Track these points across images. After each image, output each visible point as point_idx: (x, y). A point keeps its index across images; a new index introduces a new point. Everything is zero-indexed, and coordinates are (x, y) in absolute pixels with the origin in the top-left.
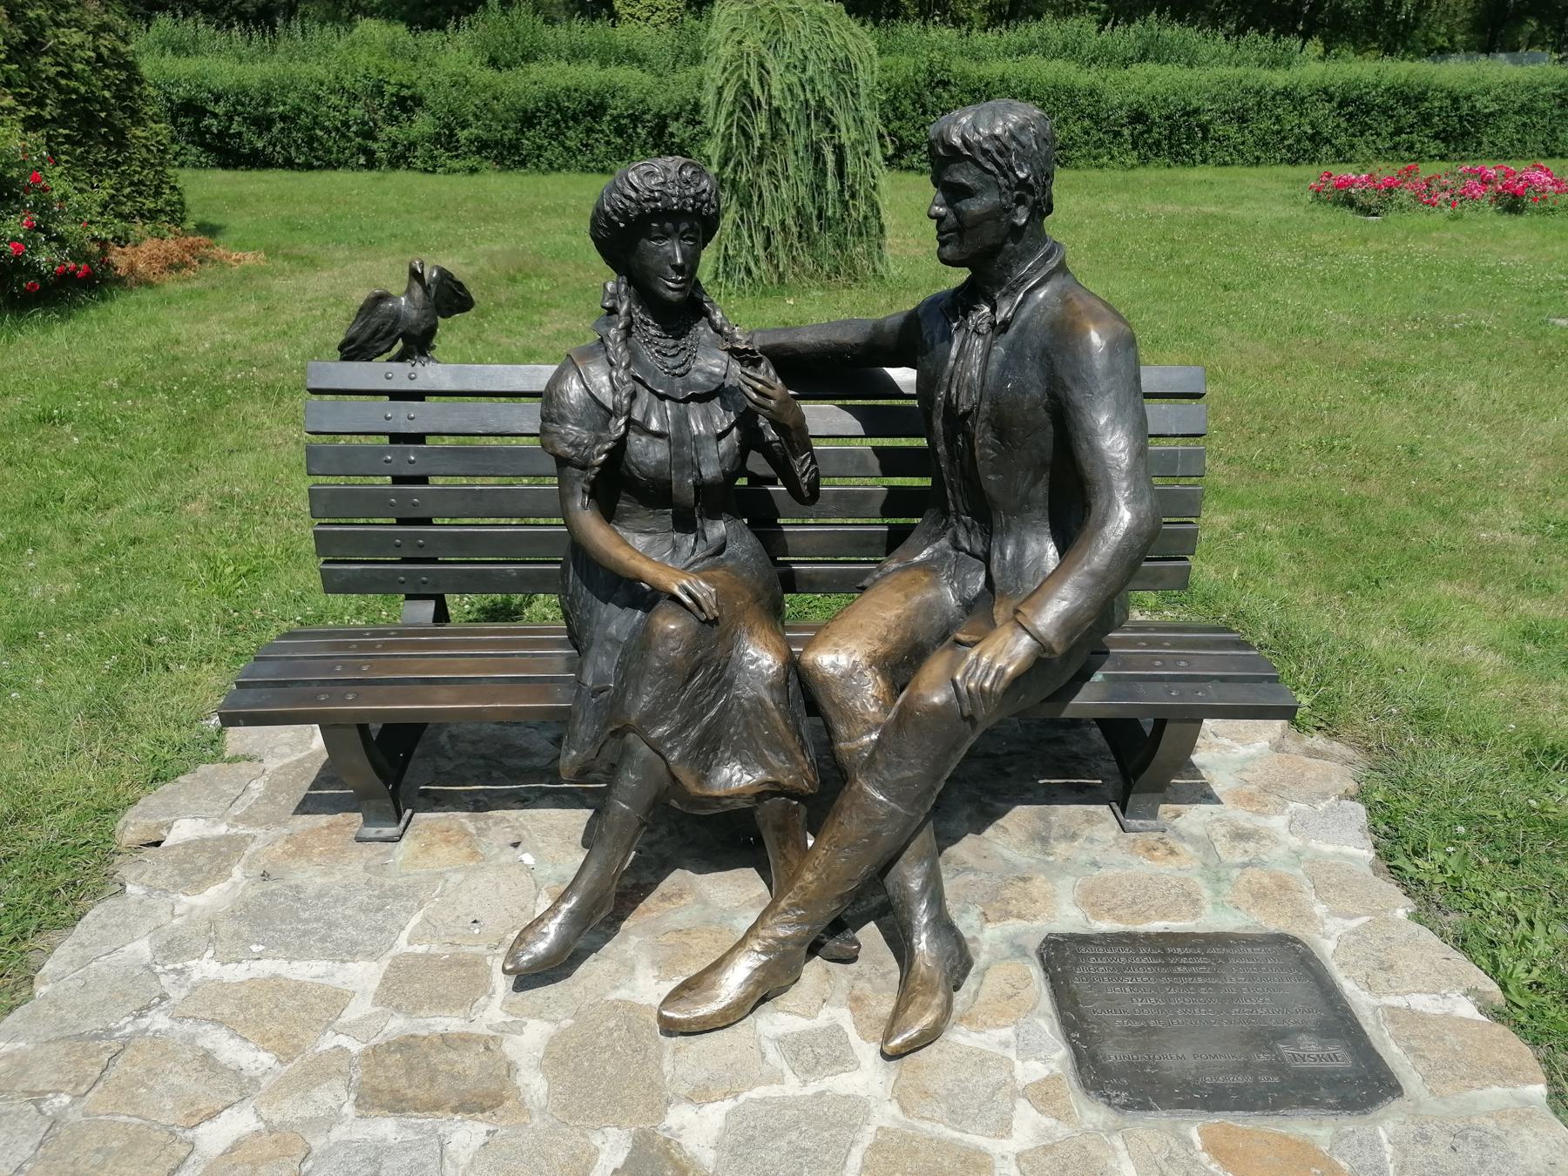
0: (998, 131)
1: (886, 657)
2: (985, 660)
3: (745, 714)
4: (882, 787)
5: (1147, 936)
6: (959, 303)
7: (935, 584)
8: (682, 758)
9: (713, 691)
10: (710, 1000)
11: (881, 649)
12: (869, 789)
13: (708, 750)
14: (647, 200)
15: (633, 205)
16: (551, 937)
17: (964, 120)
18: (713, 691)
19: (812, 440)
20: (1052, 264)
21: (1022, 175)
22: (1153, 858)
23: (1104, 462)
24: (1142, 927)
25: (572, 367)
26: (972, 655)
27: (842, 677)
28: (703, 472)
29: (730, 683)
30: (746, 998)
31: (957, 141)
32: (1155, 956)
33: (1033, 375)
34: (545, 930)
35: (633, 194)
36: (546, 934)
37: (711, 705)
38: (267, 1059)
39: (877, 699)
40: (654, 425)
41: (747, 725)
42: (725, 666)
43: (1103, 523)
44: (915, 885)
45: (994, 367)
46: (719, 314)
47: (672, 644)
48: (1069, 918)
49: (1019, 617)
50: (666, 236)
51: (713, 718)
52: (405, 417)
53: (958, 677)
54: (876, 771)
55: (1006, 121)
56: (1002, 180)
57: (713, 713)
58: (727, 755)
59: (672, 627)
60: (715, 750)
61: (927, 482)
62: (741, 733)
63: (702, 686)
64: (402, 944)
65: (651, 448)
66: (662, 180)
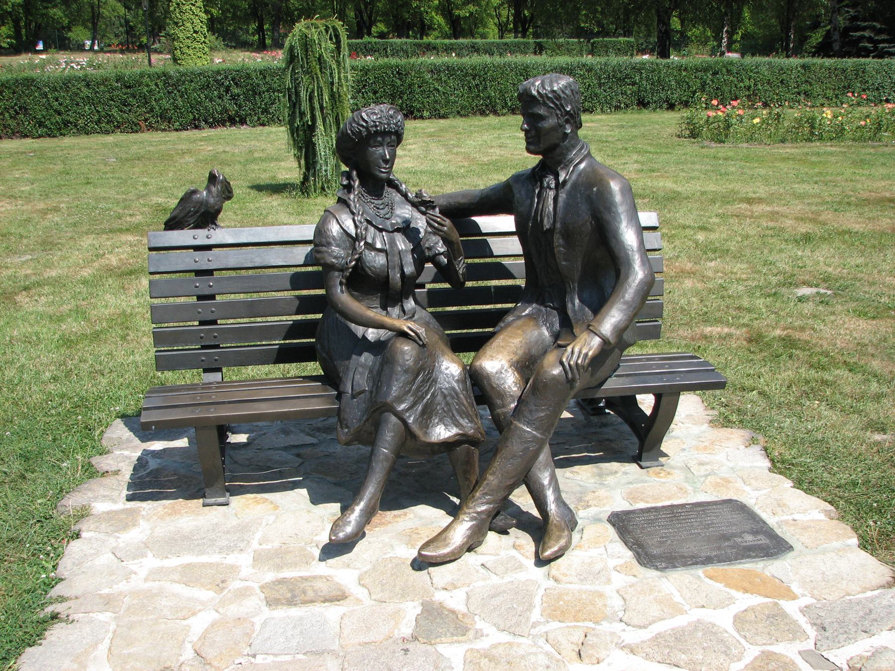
0: (555, 89)
1: (518, 362)
2: (577, 350)
3: (445, 397)
4: (529, 424)
5: (663, 507)
6: (536, 176)
7: (538, 326)
8: (415, 421)
9: (428, 384)
10: (447, 545)
11: (514, 359)
12: (521, 426)
13: (427, 415)
14: (372, 127)
15: (364, 130)
16: (353, 523)
17: (537, 84)
18: (428, 384)
20: (584, 152)
21: (568, 109)
22: (659, 477)
23: (624, 247)
24: (660, 504)
25: (331, 216)
26: (569, 349)
27: (496, 373)
28: (405, 270)
29: (435, 381)
30: (463, 544)
31: (534, 93)
32: (670, 514)
33: (584, 208)
34: (348, 520)
35: (364, 124)
36: (350, 522)
37: (427, 392)
38: (211, 594)
39: (516, 384)
40: (379, 245)
41: (447, 404)
42: (433, 370)
43: (627, 277)
44: (546, 482)
45: (649, 149)
46: (404, 186)
48: (622, 505)
49: (591, 328)
50: (381, 145)
51: (428, 399)
52: (203, 261)
53: (564, 360)
54: (524, 416)
55: (558, 84)
56: (558, 112)
57: (428, 397)
58: (436, 421)
59: (406, 348)
60: (430, 418)
62: (443, 408)
63: (423, 381)
64: (255, 545)
65: (377, 258)
66: (379, 116)
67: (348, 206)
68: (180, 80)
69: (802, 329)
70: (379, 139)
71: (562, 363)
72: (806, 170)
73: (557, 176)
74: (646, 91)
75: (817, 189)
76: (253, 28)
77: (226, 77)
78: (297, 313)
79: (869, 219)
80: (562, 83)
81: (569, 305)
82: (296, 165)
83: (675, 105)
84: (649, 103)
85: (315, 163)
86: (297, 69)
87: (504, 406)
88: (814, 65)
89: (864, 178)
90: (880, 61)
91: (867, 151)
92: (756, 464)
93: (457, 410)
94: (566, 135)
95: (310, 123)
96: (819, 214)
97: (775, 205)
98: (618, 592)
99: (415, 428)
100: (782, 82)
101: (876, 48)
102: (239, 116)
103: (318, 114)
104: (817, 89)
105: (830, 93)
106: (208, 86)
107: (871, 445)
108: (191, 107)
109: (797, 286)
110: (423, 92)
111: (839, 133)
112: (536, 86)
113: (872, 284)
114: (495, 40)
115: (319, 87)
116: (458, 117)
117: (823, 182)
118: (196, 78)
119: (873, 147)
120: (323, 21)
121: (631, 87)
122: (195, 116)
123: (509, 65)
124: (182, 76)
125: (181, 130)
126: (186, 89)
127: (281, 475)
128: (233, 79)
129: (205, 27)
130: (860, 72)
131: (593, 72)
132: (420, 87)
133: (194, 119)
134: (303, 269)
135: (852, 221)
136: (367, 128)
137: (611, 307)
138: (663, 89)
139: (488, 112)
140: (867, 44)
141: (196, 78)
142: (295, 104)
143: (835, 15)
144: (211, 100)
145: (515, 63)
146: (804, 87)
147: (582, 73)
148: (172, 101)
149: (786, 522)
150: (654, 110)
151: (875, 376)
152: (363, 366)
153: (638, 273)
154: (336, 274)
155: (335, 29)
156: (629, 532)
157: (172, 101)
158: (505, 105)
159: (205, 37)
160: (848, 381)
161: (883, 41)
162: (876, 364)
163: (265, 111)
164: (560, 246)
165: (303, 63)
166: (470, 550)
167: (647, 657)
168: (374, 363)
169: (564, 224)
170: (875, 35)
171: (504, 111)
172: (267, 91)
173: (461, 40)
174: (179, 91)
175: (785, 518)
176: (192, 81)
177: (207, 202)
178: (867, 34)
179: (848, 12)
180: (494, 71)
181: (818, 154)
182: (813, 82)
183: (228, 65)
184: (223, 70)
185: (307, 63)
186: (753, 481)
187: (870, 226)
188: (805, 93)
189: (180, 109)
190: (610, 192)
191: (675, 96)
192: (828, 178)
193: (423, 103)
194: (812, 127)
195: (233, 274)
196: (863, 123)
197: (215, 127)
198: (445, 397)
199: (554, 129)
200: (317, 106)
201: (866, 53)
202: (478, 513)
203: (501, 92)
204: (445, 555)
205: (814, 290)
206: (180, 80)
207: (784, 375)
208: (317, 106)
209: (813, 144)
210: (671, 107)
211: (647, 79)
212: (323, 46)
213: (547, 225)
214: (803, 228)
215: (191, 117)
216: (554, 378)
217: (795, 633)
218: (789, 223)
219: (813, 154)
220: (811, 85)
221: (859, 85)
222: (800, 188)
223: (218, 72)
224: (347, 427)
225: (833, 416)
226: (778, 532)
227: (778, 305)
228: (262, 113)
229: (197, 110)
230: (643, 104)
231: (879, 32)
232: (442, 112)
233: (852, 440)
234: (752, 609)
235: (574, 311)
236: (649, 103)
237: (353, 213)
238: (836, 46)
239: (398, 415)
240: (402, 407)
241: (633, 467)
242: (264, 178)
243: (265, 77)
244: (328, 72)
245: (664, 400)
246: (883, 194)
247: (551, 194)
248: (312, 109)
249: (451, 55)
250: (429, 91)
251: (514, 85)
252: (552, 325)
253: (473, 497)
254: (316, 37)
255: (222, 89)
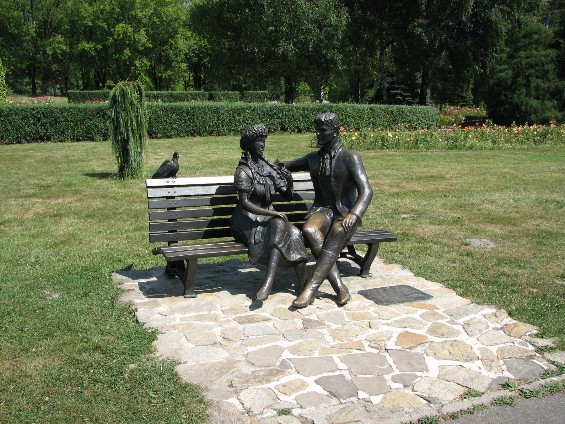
1: (321, 228)
2: (348, 221)
3: (295, 242)
4: (331, 251)
6: (320, 155)
11: (320, 227)
19: (310, 178)
20: (341, 144)
24: (376, 288)
26: (345, 220)
29: (290, 236)
31: (323, 120)
33: (343, 166)
43: (364, 193)
47: (281, 225)
61: (228, 227)
67: (248, 166)
68: (9, 113)
69: (409, 230)
70: (260, 138)
71: (342, 226)
72: (385, 163)
73: (330, 154)
74: (285, 122)
75: (395, 172)
76: (26, 82)
77: (39, 112)
78: (214, 215)
79: (424, 185)
80: (332, 116)
81: (338, 206)
82: (116, 161)
83: (302, 130)
84: (287, 129)
85: (128, 160)
86: (118, 108)
87: (317, 246)
88: (376, 108)
89: (416, 167)
90: (410, 107)
91: (413, 154)
92: (408, 274)
93: (300, 248)
94: (334, 137)
95: (126, 138)
96: (399, 183)
97: (376, 180)
98: (374, 312)
99: (285, 254)
100: (360, 117)
101: (405, 100)
102: (46, 136)
103: (130, 133)
104: (379, 121)
105: (386, 124)
106: (27, 118)
107: (451, 268)
108: (16, 130)
109: (399, 214)
110: (157, 123)
111: (397, 145)
112: (323, 117)
113: (434, 212)
114: (180, 92)
115: (132, 119)
116: (178, 137)
117: (396, 169)
118: (19, 112)
119: (416, 152)
120: (132, 82)
121: (277, 120)
122: (18, 135)
123: (208, 107)
124: (10, 111)
125: (9, 144)
126: (13, 119)
127: (210, 287)
128: (43, 114)
129: (4, 80)
130: (400, 112)
131: (256, 111)
132: (156, 120)
133: (18, 137)
134: (215, 196)
135: (415, 186)
136: (256, 134)
137: (359, 204)
138: (295, 121)
139: (195, 134)
140: (400, 97)
141: (19, 112)
142: (117, 128)
143: (383, 81)
144: (29, 126)
145: (211, 106)
146: (372, 120)
147: (249, 112)
148: (4, 126)
149: (428, 290)
150: (291, 133)
151: (446, 245)
152: (259, 232)
153: (367, 191)
154: (246, 194)
155: (139, 87)
156: (369, 296)
157: (4, 126)
158: (205, 131)
159: (4, 87)
160: (436, 248)
161: (408, 96)
162: (445, 241)
163: (63, 133)
164: (333, 182)
165: (122, 105)
166: (310, 304)
167: (394, 326)
168: (264, 230)
169: (335, 172)
170: (404, 93)
171: (205, 134)
172: (64, 121)
173: (163, 92)
174: (8, 120)
175: (427, 289)
176: (16, 114)
177: (173, 166)
178: (399, 92)
179: (388, 79)
180: (199, 111)
181: (388, 155)
182: (377, 118)
183: (42, 105)
184: (36, 108)
185: (124, 105)
186: (410, 279)
187: (425, 188)
188: (372, 124)
189: (9, 131)
190: (354, 159)
191: (302, 125)
192: (398, 167)
193: (157, 129)
194: (383, 141)
195: (183, 198)
196: (409, 139)
197: (31, 142)
198: (295, 242)
199: (329, 135)
200: (130, 129)
201: (400, 102)
202: (313, 287)
203: (203, 122)
204: (304, 304)
205: (409, 215)
206: (9, 113)
207: (408, 246)
208: (130, 129)
209: (385, 150)
210: (300, 131)
211: (286, 115)
212: (133, 96)
213: (328, 173)
214: (394, 190)
215: (16, 136)
216: (340, 232)
217: (443, 317)
218: (386, 188)
219: (386, 155)
220: (375, 119)
221: (400, 119)
222: (387, 172)
223: (33, 109)
224: (254, 257)
225: (433, 259)
226: (426, 293)
227: (394, 221)
228: (61, 134)
229: (20, 132)
230: (284, 130)
231: (406, 91)
232: (169, 134)
233: (443, 266)
234: (426, 313)
235: (340, 208)
236: (287, 129)
237: (251, 169)
238: (385, 98)
239: (278, 249)
240: (280, 246)
241: (359, 278)
242: (87, 170)
243: (62, 113)
244: (136, 110)
245: (373, 246)
246: (427, 174)
247: (328, 161)
248: (127, 130)
249: (158, 100)
250: (161, 122)
251: (211, 118)
252: (330, 215)
253: (310, 281)
254: (129, 91)
255: (35, 120)
